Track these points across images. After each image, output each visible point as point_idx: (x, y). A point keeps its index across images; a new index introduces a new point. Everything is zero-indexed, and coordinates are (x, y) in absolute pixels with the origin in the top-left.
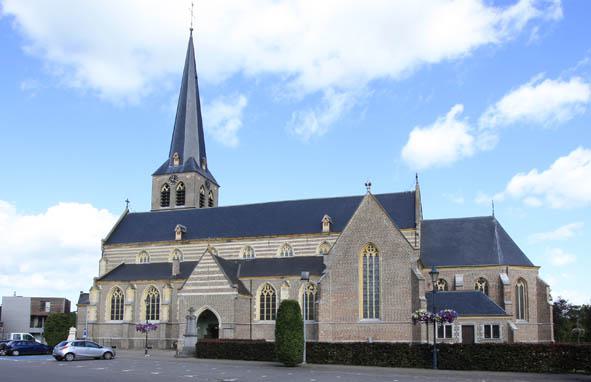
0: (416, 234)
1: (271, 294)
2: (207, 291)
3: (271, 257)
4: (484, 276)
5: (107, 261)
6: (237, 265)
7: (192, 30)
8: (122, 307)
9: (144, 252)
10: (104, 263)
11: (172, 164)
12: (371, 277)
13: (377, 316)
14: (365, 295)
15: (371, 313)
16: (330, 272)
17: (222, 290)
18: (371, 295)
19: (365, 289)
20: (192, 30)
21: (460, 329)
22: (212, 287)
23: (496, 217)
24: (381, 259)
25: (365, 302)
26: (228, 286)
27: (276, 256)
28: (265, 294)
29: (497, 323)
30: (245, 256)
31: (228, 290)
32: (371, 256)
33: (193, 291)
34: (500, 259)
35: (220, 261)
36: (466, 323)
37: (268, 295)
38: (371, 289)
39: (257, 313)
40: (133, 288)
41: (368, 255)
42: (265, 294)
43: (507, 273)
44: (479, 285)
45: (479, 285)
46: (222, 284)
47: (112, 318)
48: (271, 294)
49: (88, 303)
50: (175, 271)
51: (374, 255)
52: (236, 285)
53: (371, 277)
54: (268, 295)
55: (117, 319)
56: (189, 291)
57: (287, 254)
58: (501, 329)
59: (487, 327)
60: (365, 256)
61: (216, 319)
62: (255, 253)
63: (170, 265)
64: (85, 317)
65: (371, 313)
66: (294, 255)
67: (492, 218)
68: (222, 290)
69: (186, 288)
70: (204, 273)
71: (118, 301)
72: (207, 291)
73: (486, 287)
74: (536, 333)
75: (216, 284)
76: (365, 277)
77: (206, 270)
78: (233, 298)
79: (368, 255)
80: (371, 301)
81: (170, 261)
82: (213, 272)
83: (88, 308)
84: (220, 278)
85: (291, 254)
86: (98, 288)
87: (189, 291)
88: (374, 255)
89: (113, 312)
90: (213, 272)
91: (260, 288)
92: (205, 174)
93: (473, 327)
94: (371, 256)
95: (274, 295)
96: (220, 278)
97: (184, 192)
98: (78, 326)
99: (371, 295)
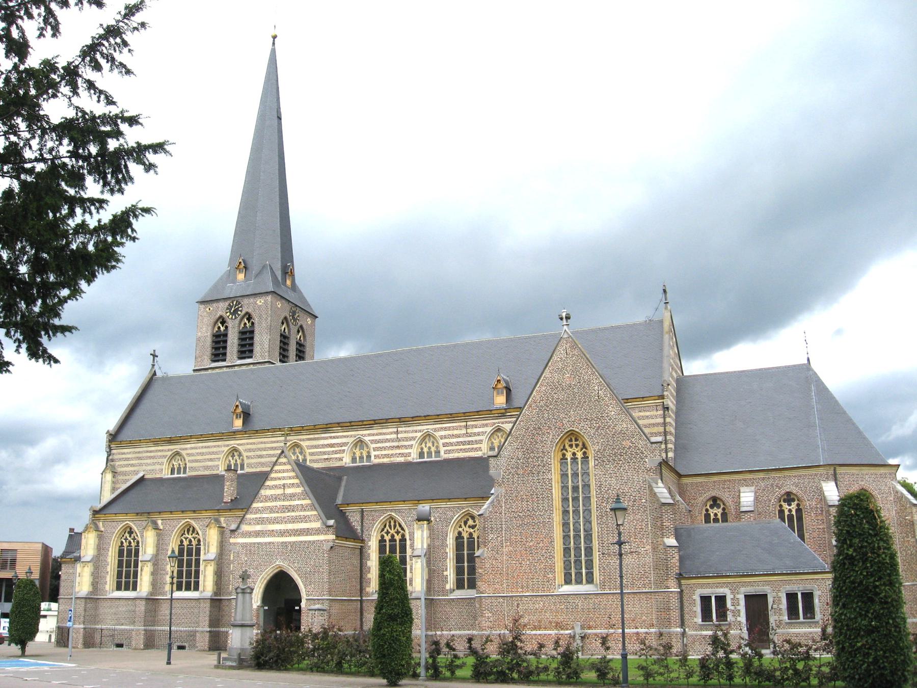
0: (666, 409)
1: (397, 538)
2: (282, 533)
3: (401, 459)
4: (794, 490)
5: (115, 473)
6: (340, 479)
7: (275, 37)
8: (136, 566)
9: (178, 453)
10: (109, 476)
11: (234, 281)
12: (575, 499)
13: (590, 580)
14: (566, 537)
15: (579, 574)
16: (502, 490)
17: (307, 532)
18: (577, 536)
19: (565, 525)
20: (275, 37)
21: (742, 602)
22: (290, 526)
23: (814, 365)
24: (592, 463)
25: (567, 551)
26: (317, 525)
27: (410, 459)
28: (387, 538)
29: (808, 587)
30: (354, 460)
31: (317, 532)
32: (574, 459)
33: (258, 534)
34: (192, 588)
35: (307, 474)
36: (751, 590)
37: (393, 539)
38: (576, 523)
39: (450, 574)
40: (156, 528)
41: (569, 456)
42: (387, 538)
43: (836, 480)
44: (786, 506)
45: (786, 506)
46: (305, 519)
47: (119, 588)
48: (397, 538)
49: (78, 559)
50: (229, 492)
51: (579, 455)
52: (331, 522)
53: (575, 499)
54: (393, 539)
55: (127, 589)
56: (249, 534)
57: (429, 454)
58: (816, 601)
59: (791, 598)
60: (564, 457)
61: (798, 536)
62: (373, 453)
63: (217, 480)
64: (73, 587)
65: (579, 574)
66: (444, 456)
67: (807, 366)
68: (307, 532)
69: (245, 528)
70: (276, 498)
71: (129, 551)
72: (282, 533)
73: (799, 511)
74: (207, 623)
75: (294, 520)
76: (565, 500)
77: (280, 491)
78: (326, 547)
79: (569, 456)
80: (577, 549)
81: (221, 471)
82: (292, 496)
83: (79, 566)
84: (303, 508)
85: (438, 452)
86: (97, 529)
87: (249, 534)
88: (579, 455)
89: (119, 575)
90: (292, 496)
91: (378, 525)
92: (291, 296)
93: (764, 596)
94: (574, 459)
95: (403, 539)
96: (303, 508)
97: (252, 332)
98: (60, 601)
99: (577, 536)
